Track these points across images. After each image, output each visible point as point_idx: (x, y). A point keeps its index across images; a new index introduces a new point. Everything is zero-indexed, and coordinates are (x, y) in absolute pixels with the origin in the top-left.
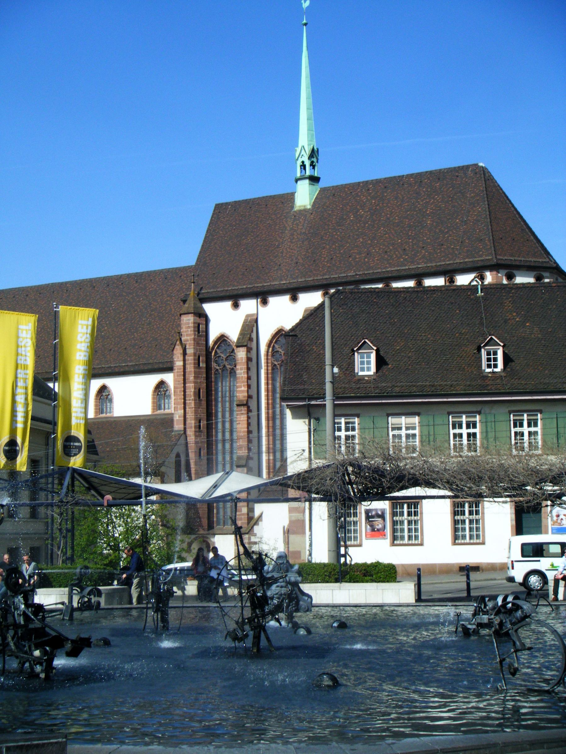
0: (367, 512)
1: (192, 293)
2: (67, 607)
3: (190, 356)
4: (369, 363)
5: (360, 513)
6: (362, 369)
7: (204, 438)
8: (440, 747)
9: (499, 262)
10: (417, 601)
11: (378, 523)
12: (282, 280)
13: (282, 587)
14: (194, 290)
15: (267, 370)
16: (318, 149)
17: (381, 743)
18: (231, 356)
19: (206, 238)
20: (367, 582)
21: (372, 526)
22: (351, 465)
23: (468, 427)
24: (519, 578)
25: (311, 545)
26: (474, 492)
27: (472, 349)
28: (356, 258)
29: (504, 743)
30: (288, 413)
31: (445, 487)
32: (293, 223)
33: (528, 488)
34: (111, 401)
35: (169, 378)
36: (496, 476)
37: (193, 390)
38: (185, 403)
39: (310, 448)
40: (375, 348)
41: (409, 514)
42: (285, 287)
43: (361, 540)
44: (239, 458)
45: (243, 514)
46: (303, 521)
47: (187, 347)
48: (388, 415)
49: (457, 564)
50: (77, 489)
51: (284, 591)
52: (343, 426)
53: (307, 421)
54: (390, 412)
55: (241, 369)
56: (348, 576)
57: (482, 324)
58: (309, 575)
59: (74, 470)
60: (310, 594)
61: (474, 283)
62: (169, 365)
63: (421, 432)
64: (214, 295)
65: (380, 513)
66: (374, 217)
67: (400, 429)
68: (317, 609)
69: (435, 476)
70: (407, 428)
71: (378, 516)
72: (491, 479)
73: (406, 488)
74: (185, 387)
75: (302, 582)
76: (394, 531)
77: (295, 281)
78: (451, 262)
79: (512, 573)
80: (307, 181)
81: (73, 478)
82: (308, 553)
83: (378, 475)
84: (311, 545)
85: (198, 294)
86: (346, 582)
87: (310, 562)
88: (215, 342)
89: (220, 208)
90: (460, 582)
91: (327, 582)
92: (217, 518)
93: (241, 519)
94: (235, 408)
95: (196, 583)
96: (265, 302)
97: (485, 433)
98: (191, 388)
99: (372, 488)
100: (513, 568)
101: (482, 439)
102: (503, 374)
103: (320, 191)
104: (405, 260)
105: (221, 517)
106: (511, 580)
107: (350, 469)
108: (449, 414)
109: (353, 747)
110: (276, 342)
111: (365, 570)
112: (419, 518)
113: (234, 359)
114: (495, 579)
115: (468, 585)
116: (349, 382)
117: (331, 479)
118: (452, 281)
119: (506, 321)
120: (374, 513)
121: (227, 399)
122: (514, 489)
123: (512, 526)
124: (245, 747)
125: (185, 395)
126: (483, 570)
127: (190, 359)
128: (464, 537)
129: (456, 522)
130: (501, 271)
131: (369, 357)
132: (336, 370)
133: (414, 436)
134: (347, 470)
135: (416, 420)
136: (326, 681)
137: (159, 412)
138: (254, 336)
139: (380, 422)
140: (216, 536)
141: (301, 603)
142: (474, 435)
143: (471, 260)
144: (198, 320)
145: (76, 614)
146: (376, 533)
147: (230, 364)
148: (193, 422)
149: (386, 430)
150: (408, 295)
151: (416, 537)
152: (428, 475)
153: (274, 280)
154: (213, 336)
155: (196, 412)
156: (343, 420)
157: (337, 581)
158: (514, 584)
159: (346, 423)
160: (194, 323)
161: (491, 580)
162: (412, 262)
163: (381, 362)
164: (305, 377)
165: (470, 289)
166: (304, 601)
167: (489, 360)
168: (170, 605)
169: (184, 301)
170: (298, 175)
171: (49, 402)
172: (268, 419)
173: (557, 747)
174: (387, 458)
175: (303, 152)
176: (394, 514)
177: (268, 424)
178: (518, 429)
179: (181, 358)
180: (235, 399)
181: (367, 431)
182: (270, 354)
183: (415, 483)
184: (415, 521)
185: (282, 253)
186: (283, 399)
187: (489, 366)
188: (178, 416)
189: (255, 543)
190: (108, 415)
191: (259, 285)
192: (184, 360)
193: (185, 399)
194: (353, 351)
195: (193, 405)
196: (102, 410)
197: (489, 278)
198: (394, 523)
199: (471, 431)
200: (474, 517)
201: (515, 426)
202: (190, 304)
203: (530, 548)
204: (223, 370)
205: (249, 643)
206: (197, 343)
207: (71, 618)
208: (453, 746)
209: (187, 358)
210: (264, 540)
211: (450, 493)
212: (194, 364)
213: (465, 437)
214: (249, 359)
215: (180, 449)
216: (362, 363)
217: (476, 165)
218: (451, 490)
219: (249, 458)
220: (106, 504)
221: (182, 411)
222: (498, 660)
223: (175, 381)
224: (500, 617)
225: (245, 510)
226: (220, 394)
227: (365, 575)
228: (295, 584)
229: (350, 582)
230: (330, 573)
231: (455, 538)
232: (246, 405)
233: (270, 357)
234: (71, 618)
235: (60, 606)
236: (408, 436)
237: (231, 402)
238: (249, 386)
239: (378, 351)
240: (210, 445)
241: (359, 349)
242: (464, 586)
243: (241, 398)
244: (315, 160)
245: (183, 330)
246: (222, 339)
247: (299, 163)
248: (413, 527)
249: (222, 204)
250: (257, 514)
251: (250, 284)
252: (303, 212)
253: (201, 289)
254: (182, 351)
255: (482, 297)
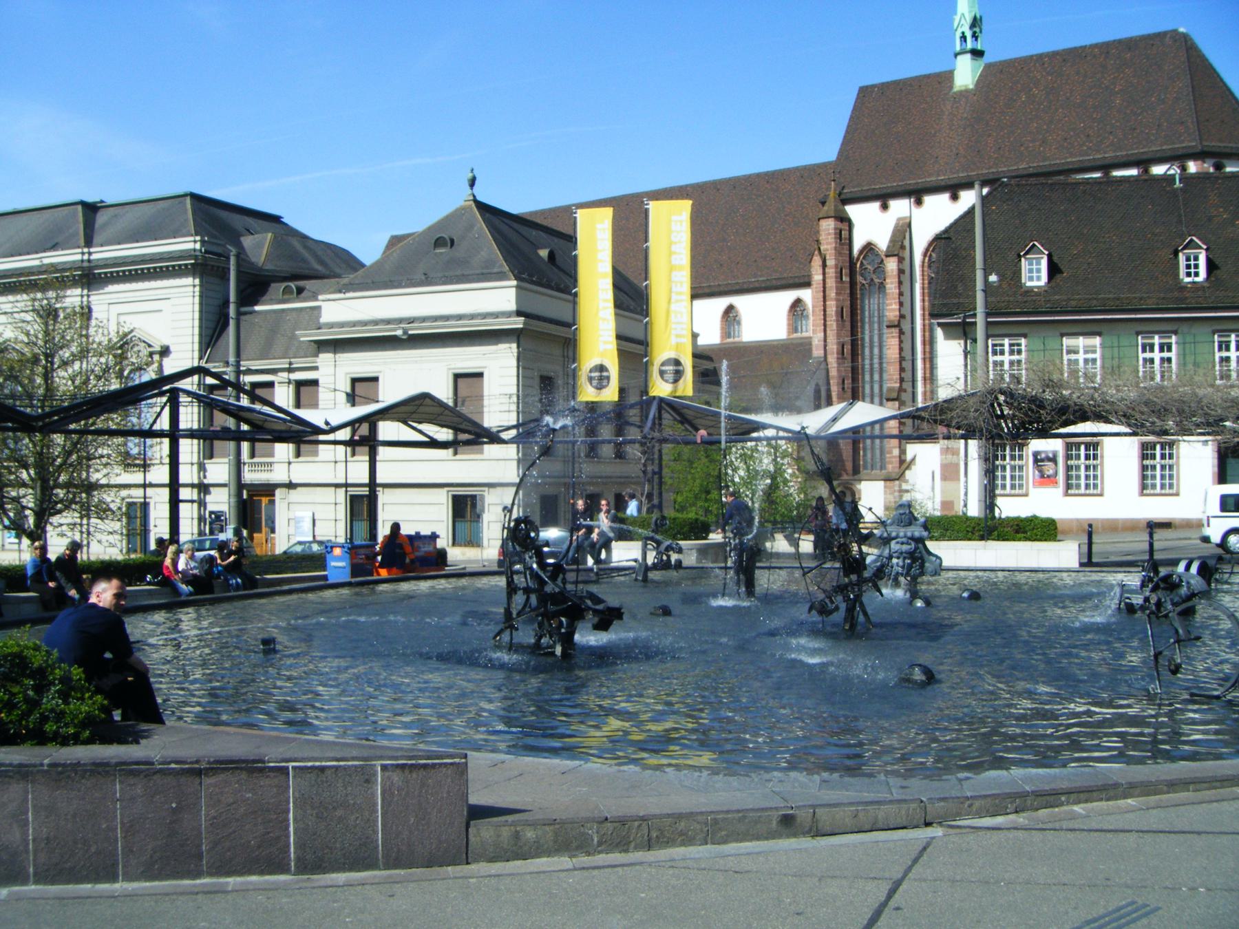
0: (1036, 454)
1: (832, 194)
2: (640, 564)
3: (831, 268)
4: (1039, 271)
5: (1027, 455)
6: (1031, 279)
7: (848, 364)
8: (1033, 788)
9: (1205, 149)
10: (1081, 565)
11: (1049, 468)
12: (939, 175)
13: (902, 543)
14: (835, 190)
15: (923, 284)
16: (981, 17)
17: (950, 777)
18: (880, 268)
19: (848, 126)
20: (1019, 540)
21: (1041, 471)
22: (1002, 392)
23: (1161, 350)
24: (1216, 538)
25: (966, 494)
26: (1157, 429)
27: (1166, 253)
28: (1028, 147)
29: (1130, 783)
30: (939, 333)
31: (1120, 421)
32: (952, 107)
33: (1227, 424)
34: (739, 323)
35: (806, 295)
36: (1187, 409)
37: (834, 309)
38: (825, 325)
39: (966, 376)
40: (1046, 252)
41: (1087, 457)
42: (943, 183)
43: (1027, 489)
44: (890, 390)
45: (895, 457)
46: (957, 465)
47: (828, 257)
48: (1062, 335)
49: (1144, 519)
50: (664, 422)
51: (905, 548)
52: (1007, 348)
53: (962, 342)
54: (1065, 331)
55: (892, 283)
56: (996, 533)
57: (1180, 222)
58: (947, 530)
59: (661, 400)
60: (939, 555)
61: (1172, 172)
62: (806, 280)
63: (1103, 357)
64: (859, 195)
65: (1051, 455)
66: (1051, 97)
67: (1076, 352)
68: (950, 574)
69: (1108, 407)
70: (1086, 352)
71: (1049, 459)
72: (1181, 412)
73: (1074, 423)
74: (825, 306)
75: (931, 538)
76: (1068, 477)
77: (955, 176)
78: (1146, 150)
79: (1207, 531)
80: (968, 56)
81: (660, 409)
82: (962, 503)
83: (1036, 405)
84: (966, 494)
85: (840, 194)
86: (994, 540)
87: (965, 514)
88: (861, 252)
89: (864, 92)
90: (1139, 543)
91: (970, 539)
92: (864, 460)
93: (891, 463)
94: (885, 330)
95: (812, 537)
96: (919, 202)
97: (1183, 355)
98: (832, 307)
99: (1031, 423)
100: (1208, 525)
101: (1178, 364)
102: (1206, 285)
103: (985, 67)
104: (1089, 148)
105: (869, 460)
106: (1206, 540)
107: (1002, 398)
108: (1138, 333)
109: (905, 783)
110: (933, 251)
111: (1017, 525)
112: (1098, 462)
113: (884, 272)
114: (1190, 539)
115: (1151, 545)
116: (1015, 294)
117: (976, 411)
118: (1146, 171)
119: (1210, 219)
120: (1043, 456)
121: (876, 319)
122: (1209, 424)
123: (1213, 473)
124: (753, 775)
125: (825, 315)
126: (1176, 527)
127: (831, 272)
128: (1154, 486)
129: (1144, 468)
130: (1207, 160)
131: (1039, 263)
132: (993, 278)
133: (1094, 360)
134: (997, 398)
135: (1097, 341)
136: (918, 675)
137: (795, 335)
138: (907, 243)
139: (1052, 343)
140: (863, 482)
141: (927, 565)
142: (1169, 360)
143: (1170, 147)
144: (840, 225)
145: (654, 575)
146: (1046, 479)
147: (878, 278)
148: (835, 347)
149: (1059, 352)
150: (1088, 187)
151: (1095, 486)
152: (1099, 406)
153: (930, 175)
154: (858, 245)
155: (839, 336)
156: (1006, 342)
157: (982, 538)
158: (1209, 545)
159: (1011, 345)
160: (835, 229)
161: (1186, 539)
162: (1098, 151)
163: (1053, 270)
164: (960, 289)
165: (1168, 179)
166: (931, 562)
167: (1188, 267)
168: (758, 564)
169: (823, 203)
170: (958, 48)
171: (642, 318)
172: (924, 343)
173: (1209, 789)
174: (1049, 384)
175: (963, 21)
176: (1068, 457)
177: (924, 348)
178: (1224, 354)
179: (820, 271)
180: (885, 319)
181: (1035, 353)
182: (926, 264)
183: (1084, 418)
184: (1094, 466)
185: (939, 142)
186: (933, 316)
187: (1189, 275)
188: (817, 340)
189: (907, 491)
190: (737, 339)
191: (912, 182)
192: (824, 274)
193: (825, 320)
194: (1019, 256)
195: (835, 327)
196: (730, 334)
197: (1192, 167)
198: (1068, 468)
199: (1166, 355)
200: (1167, 462)
201: (1220, 349)
202: (829, 208)
203: (1231, 502)
204: (870, 285)
205: (838, 616)
206: (838, 252)
207: (645, 580)
208: (1053, 786)
209: (827, 270)
210: (918, 487)
211: (1128, 430)
212: (836, 277)
213: (1157, 362)
214: (901, 272)
215: (820, 375)
216: (1031, 271)
217: (1175, 31)
218: (1129, 425)
219: (901, 390)
220: (699, 441)
221: (822, 334)
222: (1152, 653)
223: (814, 298)
224: (1157, 595)
225: (896, 452)
226: (867, 313)
227: (1017, 532)
228: (920, 541)
229: (998, 540)
230: (974, 528)
231: (1143, 487)
232: (898, 326)
233: (926, 269)
234: (645, 580)
235: (633, 564)
236: (1086, 361)
237: (880, 323)
238: (901, 304)
239: (1050, 257)
240: (855, 373)
241: (1027, 253)
242: (1146, 546)
243: (892, 318)
244: (977, 30)
245: (822, 237)
246: (869, 248)
247: (958, 35)
248: (1092, 473)
249: (867, 87)
250: (909, 457)
251: (901, 181)
252: (965, 93)
253: (843, 188)
254: (821, 263)
255: (1181, 189)
